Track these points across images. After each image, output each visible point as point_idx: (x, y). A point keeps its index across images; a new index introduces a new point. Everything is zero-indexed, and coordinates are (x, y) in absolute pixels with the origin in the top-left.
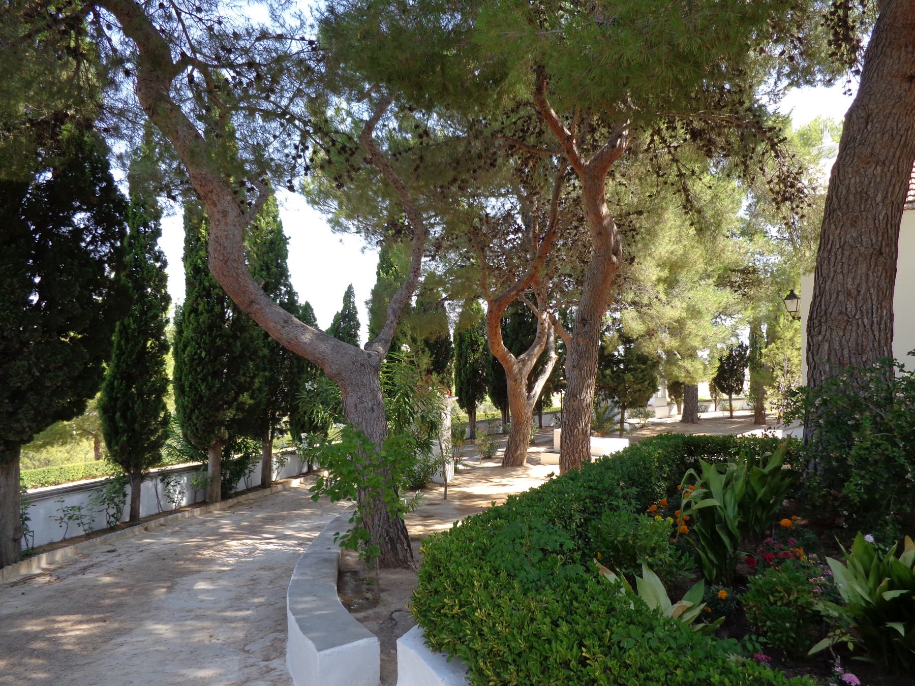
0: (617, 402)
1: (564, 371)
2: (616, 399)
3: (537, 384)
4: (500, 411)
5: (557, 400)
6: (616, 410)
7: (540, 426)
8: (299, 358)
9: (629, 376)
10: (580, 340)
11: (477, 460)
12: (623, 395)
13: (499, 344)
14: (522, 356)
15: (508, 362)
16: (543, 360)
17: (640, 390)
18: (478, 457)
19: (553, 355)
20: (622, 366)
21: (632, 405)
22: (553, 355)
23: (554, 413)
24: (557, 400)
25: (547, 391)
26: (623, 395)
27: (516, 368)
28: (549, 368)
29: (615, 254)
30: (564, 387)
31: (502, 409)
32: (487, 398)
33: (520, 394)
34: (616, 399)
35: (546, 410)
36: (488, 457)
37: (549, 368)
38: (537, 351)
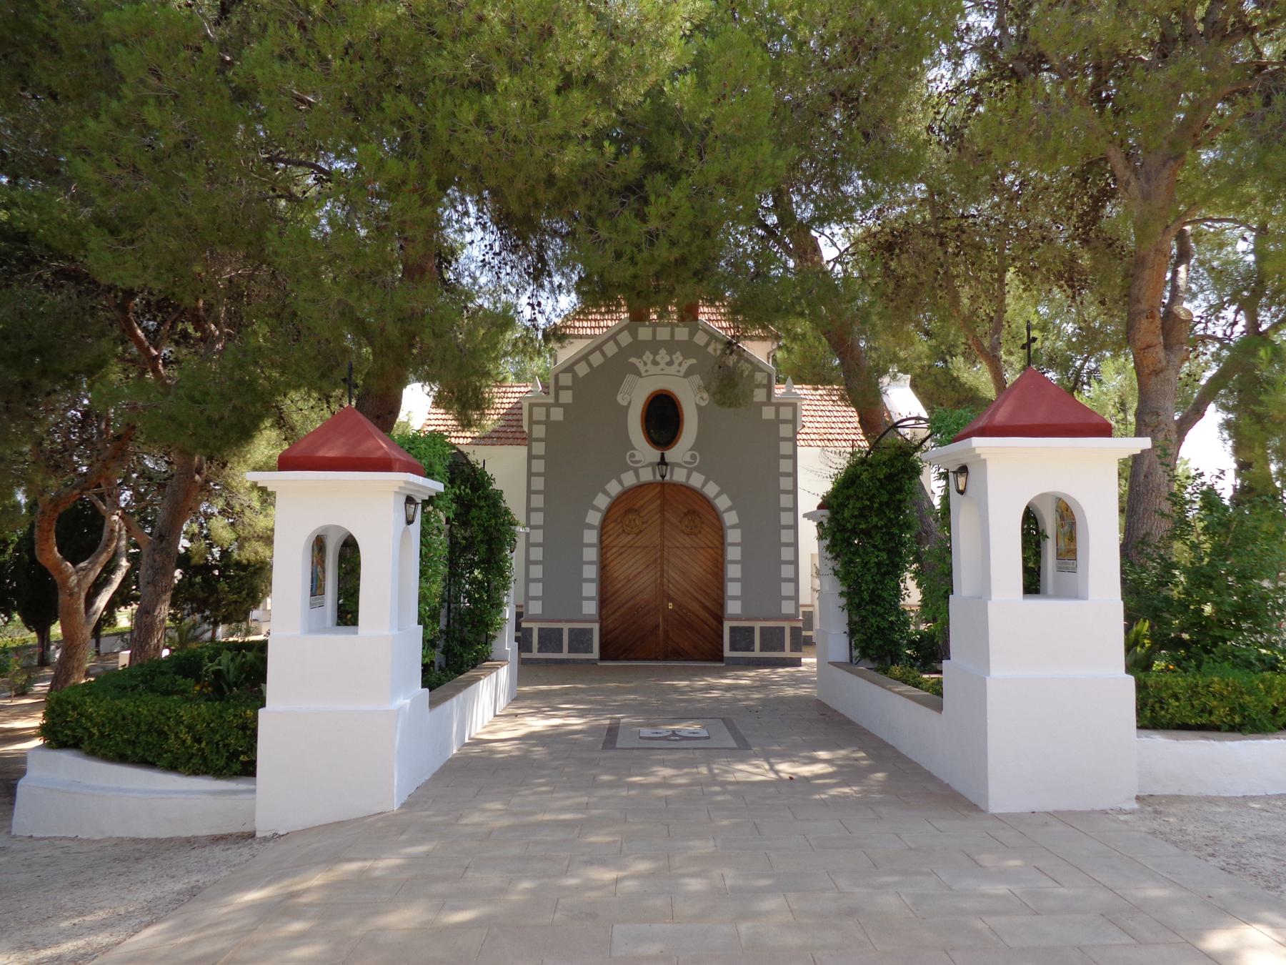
0: (207, 618)
1: (137, 577)
2: (207, 613)
3: (807, 774)
4: (34, 635)
5: (124, 619)
6: (206, 626)
7: (98, 653)
8: (346, 624)
9: (223, 586)
10: (157, 557)
11: (9, 697)
12: (216, 607)
13: (51, 551)
14: (82, 565)
15: (61, 572)
16: (110, 568)
17: (235, 602)
18: (8, 694)
19: (124, 563)
20: (216, 573)
21: (226, 620)
22: (124, 563)
23: (121, 634)
24: (124, 619)
25: (112, 606)
26: (216, 607)
27: (73, 580)
28: (118, 578)
29: (199, 473)
30: (136, 599)
31: (38, 633)
32: (1227, 502)
33: (77, 611)
34: (207, 613)
35: (107, 630)
36: (23, 693)
37: (118, 578)
38: (104, 558)
